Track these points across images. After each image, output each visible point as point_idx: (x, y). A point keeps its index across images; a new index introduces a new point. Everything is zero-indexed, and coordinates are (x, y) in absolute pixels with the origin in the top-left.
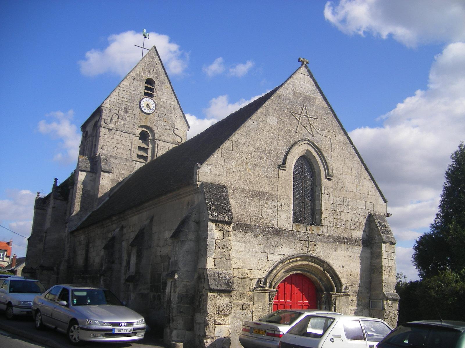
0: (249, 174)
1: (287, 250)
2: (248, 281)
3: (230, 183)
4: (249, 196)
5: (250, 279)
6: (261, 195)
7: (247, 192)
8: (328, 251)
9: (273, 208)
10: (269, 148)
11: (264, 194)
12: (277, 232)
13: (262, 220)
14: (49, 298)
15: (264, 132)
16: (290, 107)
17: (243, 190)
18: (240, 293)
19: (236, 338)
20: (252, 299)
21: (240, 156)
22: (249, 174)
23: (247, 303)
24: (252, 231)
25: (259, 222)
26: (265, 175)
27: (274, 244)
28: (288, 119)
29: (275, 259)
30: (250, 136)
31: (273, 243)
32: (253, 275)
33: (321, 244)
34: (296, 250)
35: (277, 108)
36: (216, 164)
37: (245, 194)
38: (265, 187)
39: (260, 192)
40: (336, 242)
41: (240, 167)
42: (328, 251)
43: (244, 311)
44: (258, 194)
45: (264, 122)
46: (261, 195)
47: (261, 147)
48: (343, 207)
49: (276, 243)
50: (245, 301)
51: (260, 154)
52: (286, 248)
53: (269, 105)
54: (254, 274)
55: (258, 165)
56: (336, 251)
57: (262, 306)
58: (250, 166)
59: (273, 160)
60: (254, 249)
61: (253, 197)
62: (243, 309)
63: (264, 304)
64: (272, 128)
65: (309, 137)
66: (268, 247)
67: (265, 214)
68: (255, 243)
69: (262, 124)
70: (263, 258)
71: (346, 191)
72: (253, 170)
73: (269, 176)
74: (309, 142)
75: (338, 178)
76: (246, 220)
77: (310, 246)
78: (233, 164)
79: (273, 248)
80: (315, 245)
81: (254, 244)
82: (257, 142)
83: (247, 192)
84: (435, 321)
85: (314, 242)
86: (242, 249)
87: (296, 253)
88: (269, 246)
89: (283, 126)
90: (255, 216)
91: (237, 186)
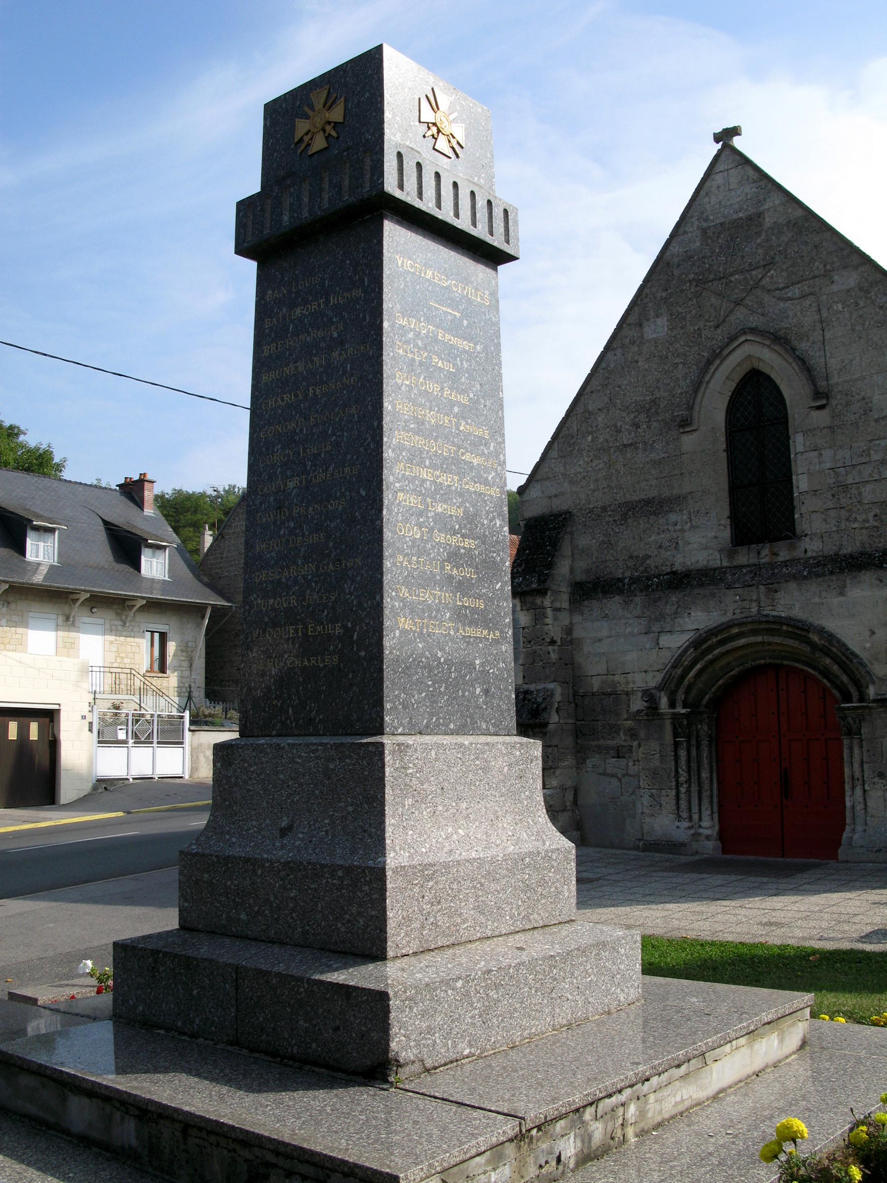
0: (614, 471)
1: (700, 618)
2: (624, 697)
3: (579, 504)
4: (616, 518)
5: (627, 694)
6: (642, 507)
7: (613, 511)
8: (817, 600)
9: (670, 528)
10: (653, 394)
11: (648, 502)
12: (682, 581)
13: (648, 562)
14: (607, 771)
15: (640, 364)
16: (696, 274)
17: (604, 509)
18: (609, 724)
19: (540, 813)
20: (633, 734)
21: (593, 440)
22: (614, 471)
23: (624, 744)
24: (620, 592)
25: (641, 569)
26: (648, 459)
27: (669, 609)
28: (693, 305)
29: (675, 641)
30: (610, 387)
31: (668, 607)
32: (631, 685)
33: (792, 585)
34: (725, 614)
35: (664, 294)
36: (550, 475)
37: (610, 516)
38: (651, 486)
39: (639, 502)
40: (842, 570)
41: (596, 462)
42: (817, 600)
43: (623, 762)
44: (637, 506)
45: (638, 343)
46: (642, 507)
47: (636, 401)
48: (867, 470)
49: (675, 607)
50: (621, 739)
51: (635, 417)
52: (700, 613)
53: (646, 297)
54: (634, 682)
55: (631, 444)
56: (842, 594)
57: (658, 749)
58: (615, 452)
59: (662, 420)
60: (629, 629)
61: (625, 517)
62: (618, 757)
63: (661, 744)
64: (656, 347)
65: (755, 321)
66: (657, 620)
67: (653, 546)
68: (629, 616)
69: (635, 349)
70: (648, 646)
71: (876, 421)
72: (621, 459)
73: (658, 457)
74: (749, 338)
75: (847, 395)
76: (613, 570)
77: (763, 598)
78: (581, 462)
79: (668, 620)
80: (776, 592)
81: (626, 618)
82: (625, 395)
83: (613, 511)
84: (121, 595)
85: (772, 584)
86: (605, 633)
87: (724, 619)
88: (661, 617)
89: (682, 328)
90: (631, 557)
91: (591, 506)
